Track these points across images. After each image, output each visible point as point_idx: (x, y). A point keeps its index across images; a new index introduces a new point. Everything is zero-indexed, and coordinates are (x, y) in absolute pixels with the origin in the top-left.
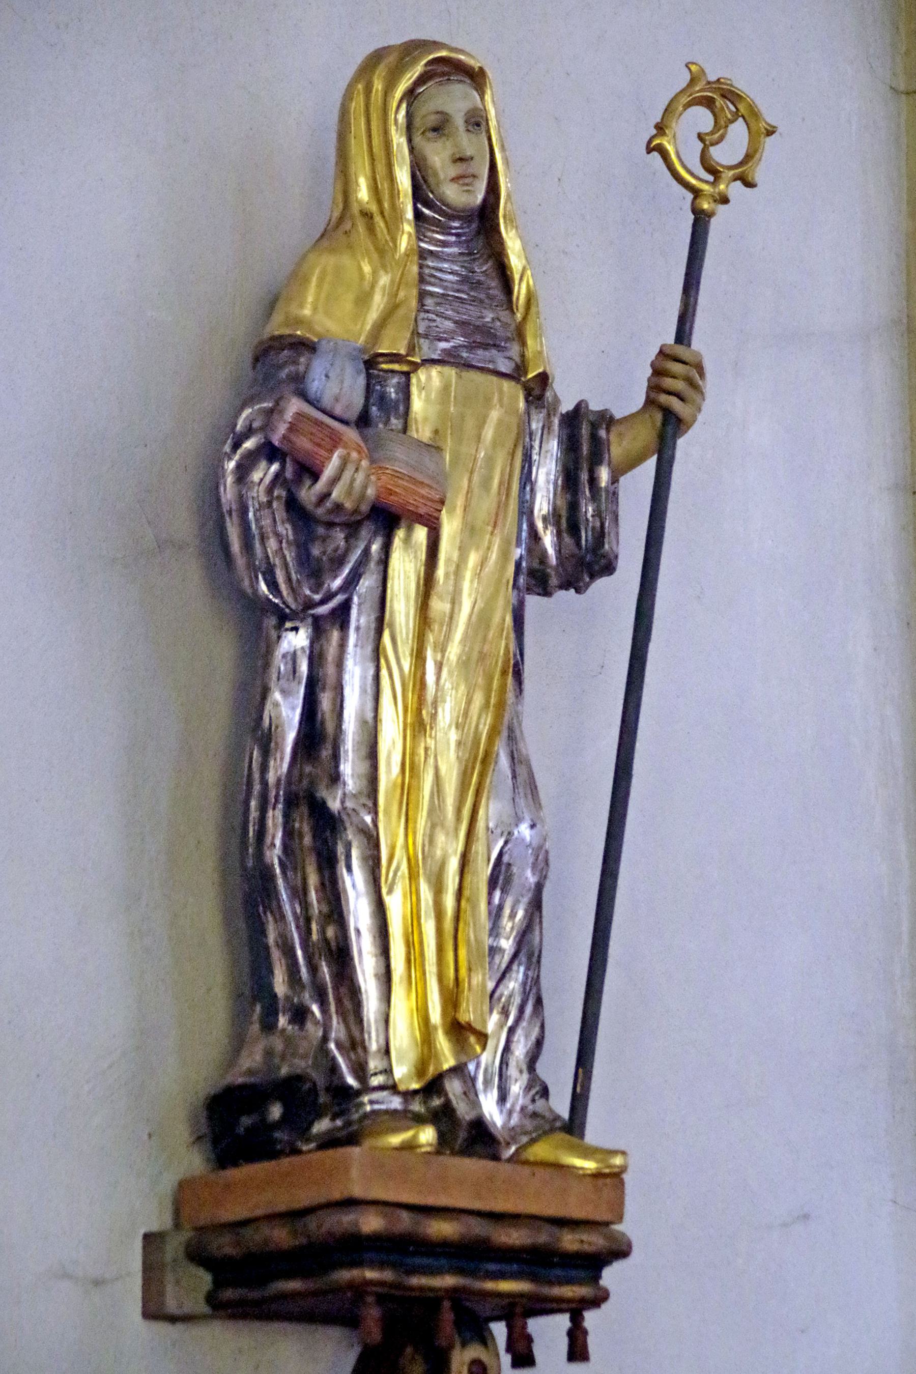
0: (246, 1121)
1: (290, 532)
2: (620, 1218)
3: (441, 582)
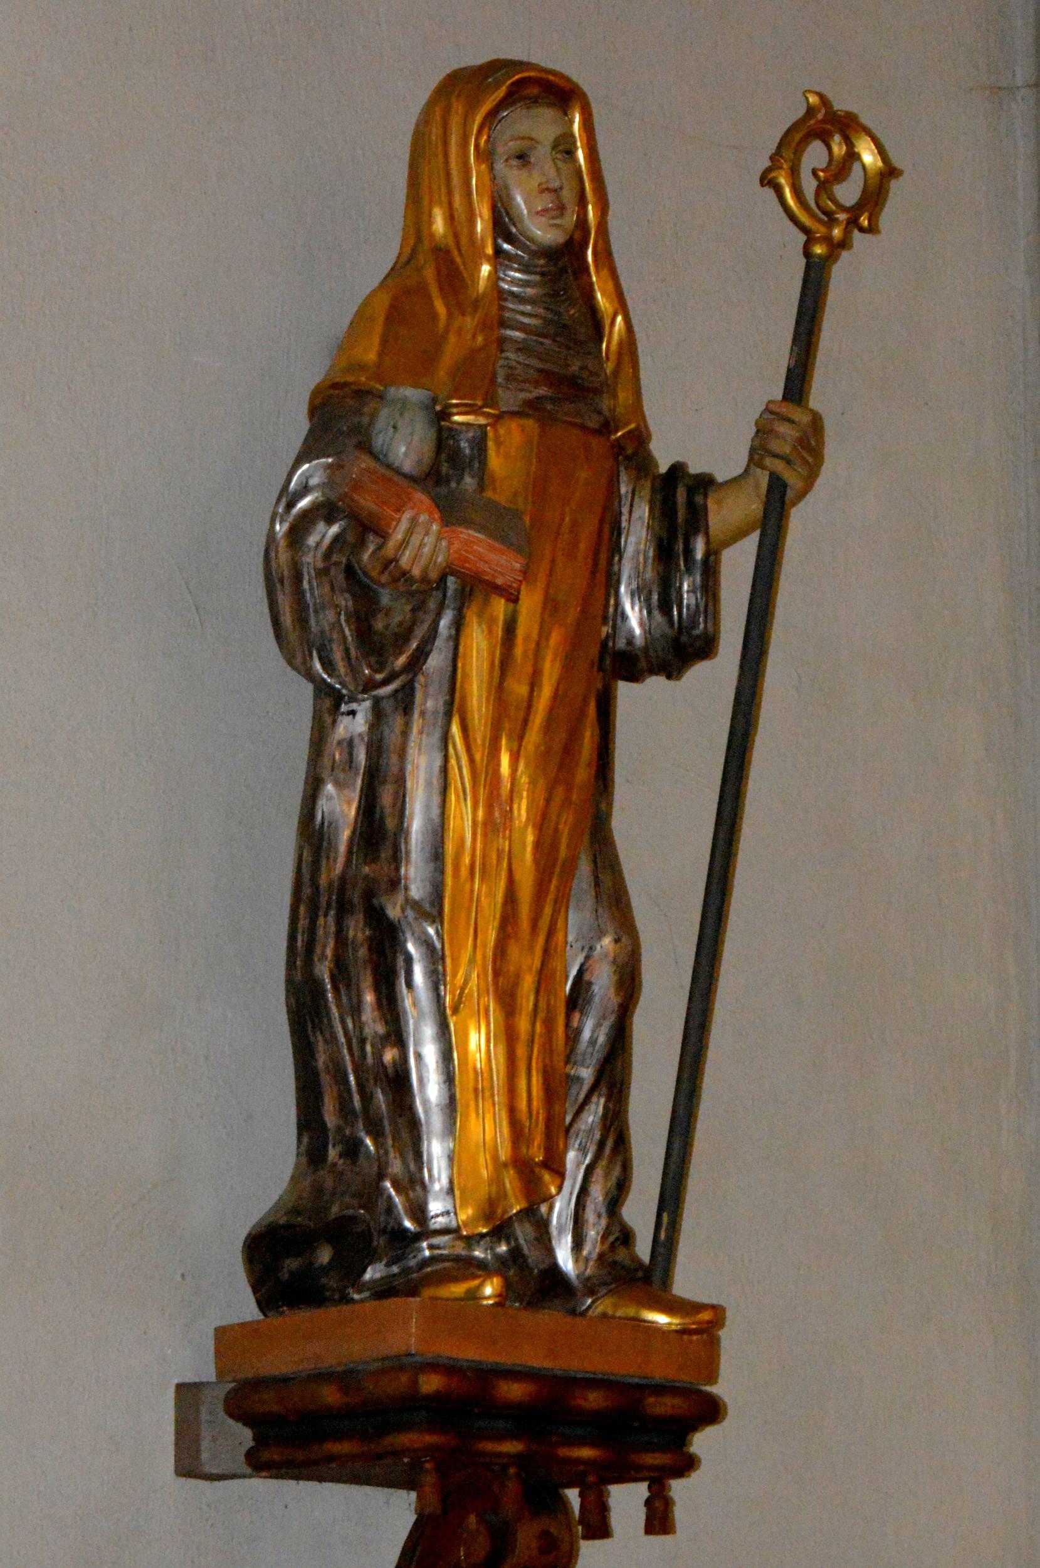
0: (292, 1264)
1: (350, 603)
2: (712, 1378)
3: (519, 661)
